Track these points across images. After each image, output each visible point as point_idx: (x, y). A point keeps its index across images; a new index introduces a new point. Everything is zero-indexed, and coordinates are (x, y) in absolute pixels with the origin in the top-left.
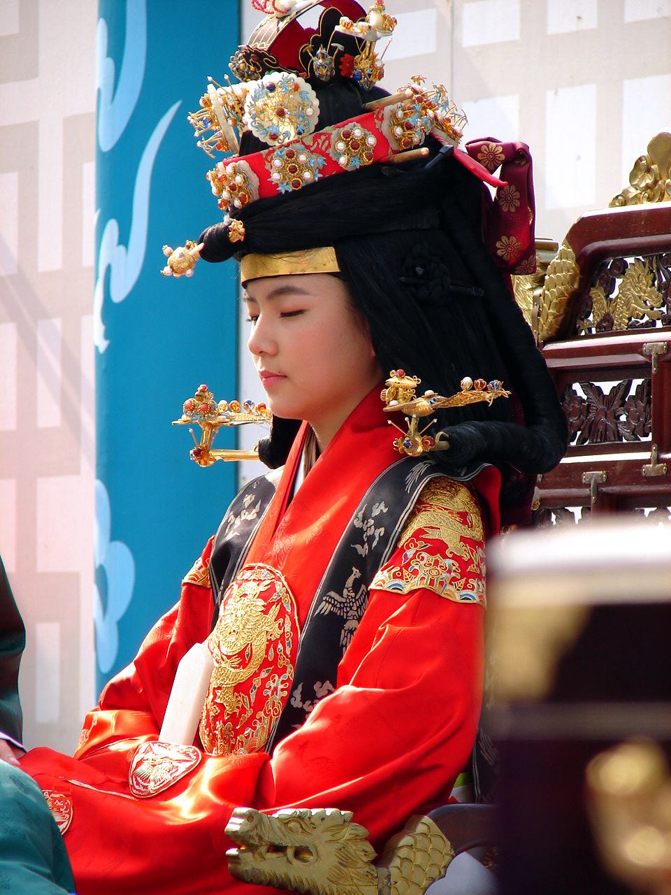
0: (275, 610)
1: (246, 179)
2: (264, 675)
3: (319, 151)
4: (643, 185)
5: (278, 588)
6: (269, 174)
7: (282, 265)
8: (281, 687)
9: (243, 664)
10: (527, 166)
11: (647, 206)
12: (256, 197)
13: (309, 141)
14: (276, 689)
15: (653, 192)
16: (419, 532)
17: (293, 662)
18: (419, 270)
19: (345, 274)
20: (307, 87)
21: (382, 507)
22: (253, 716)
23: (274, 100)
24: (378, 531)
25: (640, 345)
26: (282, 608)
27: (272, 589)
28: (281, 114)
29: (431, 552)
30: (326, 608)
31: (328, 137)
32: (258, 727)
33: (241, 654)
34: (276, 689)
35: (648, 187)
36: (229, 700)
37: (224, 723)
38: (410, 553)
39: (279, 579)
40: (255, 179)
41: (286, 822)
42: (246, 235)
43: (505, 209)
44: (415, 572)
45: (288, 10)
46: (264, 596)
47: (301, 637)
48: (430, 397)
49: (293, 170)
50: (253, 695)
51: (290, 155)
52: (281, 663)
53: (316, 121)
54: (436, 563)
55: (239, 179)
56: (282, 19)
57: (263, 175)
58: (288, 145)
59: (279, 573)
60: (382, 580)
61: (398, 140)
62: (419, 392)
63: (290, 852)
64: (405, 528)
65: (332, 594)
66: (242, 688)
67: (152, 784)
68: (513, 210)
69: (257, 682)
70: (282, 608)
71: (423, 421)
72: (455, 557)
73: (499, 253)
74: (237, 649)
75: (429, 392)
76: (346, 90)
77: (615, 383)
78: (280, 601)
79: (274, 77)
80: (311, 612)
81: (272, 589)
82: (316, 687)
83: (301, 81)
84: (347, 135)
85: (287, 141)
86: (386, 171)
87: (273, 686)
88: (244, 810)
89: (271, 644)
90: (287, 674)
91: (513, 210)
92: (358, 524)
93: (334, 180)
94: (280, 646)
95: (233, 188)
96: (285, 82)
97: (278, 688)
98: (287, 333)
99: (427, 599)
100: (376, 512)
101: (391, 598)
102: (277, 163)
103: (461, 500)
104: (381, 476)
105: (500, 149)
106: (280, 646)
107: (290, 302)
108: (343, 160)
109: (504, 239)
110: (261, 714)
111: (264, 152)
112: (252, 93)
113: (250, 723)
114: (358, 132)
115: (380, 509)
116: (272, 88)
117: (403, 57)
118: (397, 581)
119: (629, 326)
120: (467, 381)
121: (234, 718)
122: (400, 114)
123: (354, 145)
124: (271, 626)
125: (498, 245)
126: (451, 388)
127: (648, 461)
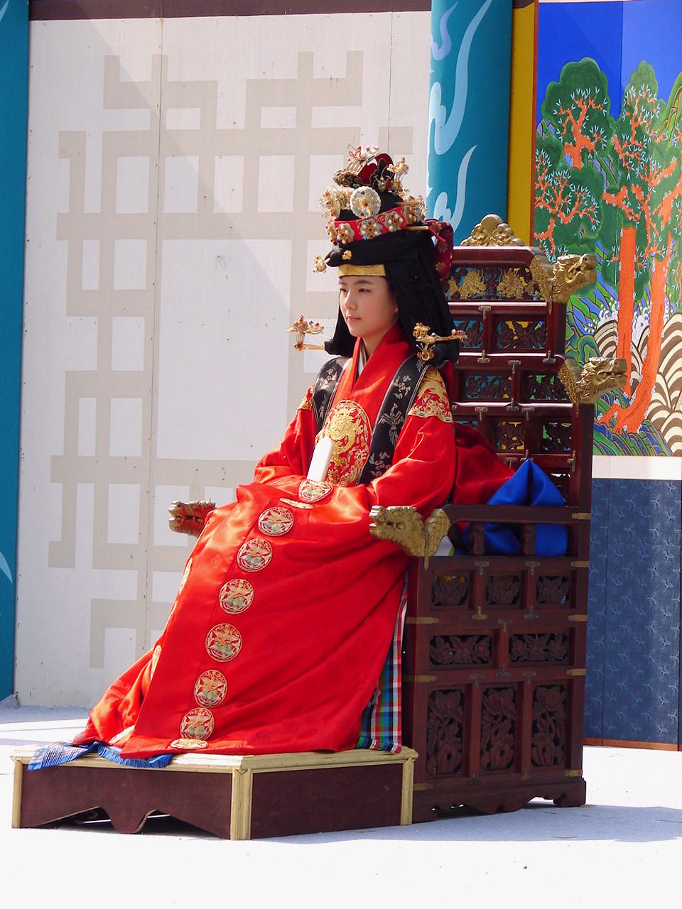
0: (358, 422)
1: (349, 232)
2: (354, 449)
3: (379, 223)
4: (479, 238)
5: (359, 412)
6: (359, 231)
7: (361, 271)
8: (363, 455)
9: (344, 444)
10: (450, 234)
12: (352, 240)
13: (376, 217)
14: (360, 456)
16: (428, 391)
17: (368, 444)
18: (416, 277)
19: (388, 277)
21: (408, 377)
23: (362, 199)
24: (407, 388)
25: (478, 306)
26: (362, 421)
27: (356, 412)
30: (383, 420)
31: (384, 216)
32: (352, 472)
34: (360, 456)
36: (337, 462)
37: (334, 470)
39: (359, 408)
41: (392, 511)
42: (351, 258)
44: (429, 409)
45: (364, 158)
47: (372, 434)
48: (434, 336)
49: (370, 230)
50: (349, 458)
52: (362, 445)
53: (379, 209)
54: (437, 405)
55: (346, 232)
56: (362, 161)
57: (357, 232)
58: (368, 219)
59: (359, 405)
61: (409, 220)
62: (429, 333)
63: (395, 525)
64: (420, 388)
65: (386, 415)
66: (343, 455)
67: (313, 497)
68: (444, 251)
69: (351, 453)
70: (362, 421)
71: (430, 345)
72: (443, 402)
73: (437, 269)
74: (340, 438)
75: (433, 334)
76: (391, 200)
77: (461, 322)
78: (361, 417)
80: (376, 423)
82: (380, 455)
83: (374, 191)
84: (393, 216)
85: (367, 217)
86: (406, 233)
87: (359, 454)
88: (378, 507)
90: (366, 449)
91: (444, 251)
92: (396, 385)
93: (386, 234)
94: (362, 437)
95: (343, 235)
96: (368, 190)
97: (361, 456)
98: (363, 300)
99: (435, 419)
100: (405, 380)
101: (418, 421)
102: (364, 226)
103: (438, 377)
104: (401, 366)
106: (362, 437)
107: (365, 287)
108: (391, 228)
109: (439, 263)
110: (353, 466)
111: (357, 221)
112: (353, 194)
113: (347, 470)
114: (397, 216)
115: (406, 378)
116: (363, 193)
118: (422, 412)
119: (468, 298)
120: (454, 331)
121: (339, 468)
122: (411, 209)
123: (396, 221)
124: (357, 428)
125: (437, 265)
126: (445, 332)
127: (481, 357)
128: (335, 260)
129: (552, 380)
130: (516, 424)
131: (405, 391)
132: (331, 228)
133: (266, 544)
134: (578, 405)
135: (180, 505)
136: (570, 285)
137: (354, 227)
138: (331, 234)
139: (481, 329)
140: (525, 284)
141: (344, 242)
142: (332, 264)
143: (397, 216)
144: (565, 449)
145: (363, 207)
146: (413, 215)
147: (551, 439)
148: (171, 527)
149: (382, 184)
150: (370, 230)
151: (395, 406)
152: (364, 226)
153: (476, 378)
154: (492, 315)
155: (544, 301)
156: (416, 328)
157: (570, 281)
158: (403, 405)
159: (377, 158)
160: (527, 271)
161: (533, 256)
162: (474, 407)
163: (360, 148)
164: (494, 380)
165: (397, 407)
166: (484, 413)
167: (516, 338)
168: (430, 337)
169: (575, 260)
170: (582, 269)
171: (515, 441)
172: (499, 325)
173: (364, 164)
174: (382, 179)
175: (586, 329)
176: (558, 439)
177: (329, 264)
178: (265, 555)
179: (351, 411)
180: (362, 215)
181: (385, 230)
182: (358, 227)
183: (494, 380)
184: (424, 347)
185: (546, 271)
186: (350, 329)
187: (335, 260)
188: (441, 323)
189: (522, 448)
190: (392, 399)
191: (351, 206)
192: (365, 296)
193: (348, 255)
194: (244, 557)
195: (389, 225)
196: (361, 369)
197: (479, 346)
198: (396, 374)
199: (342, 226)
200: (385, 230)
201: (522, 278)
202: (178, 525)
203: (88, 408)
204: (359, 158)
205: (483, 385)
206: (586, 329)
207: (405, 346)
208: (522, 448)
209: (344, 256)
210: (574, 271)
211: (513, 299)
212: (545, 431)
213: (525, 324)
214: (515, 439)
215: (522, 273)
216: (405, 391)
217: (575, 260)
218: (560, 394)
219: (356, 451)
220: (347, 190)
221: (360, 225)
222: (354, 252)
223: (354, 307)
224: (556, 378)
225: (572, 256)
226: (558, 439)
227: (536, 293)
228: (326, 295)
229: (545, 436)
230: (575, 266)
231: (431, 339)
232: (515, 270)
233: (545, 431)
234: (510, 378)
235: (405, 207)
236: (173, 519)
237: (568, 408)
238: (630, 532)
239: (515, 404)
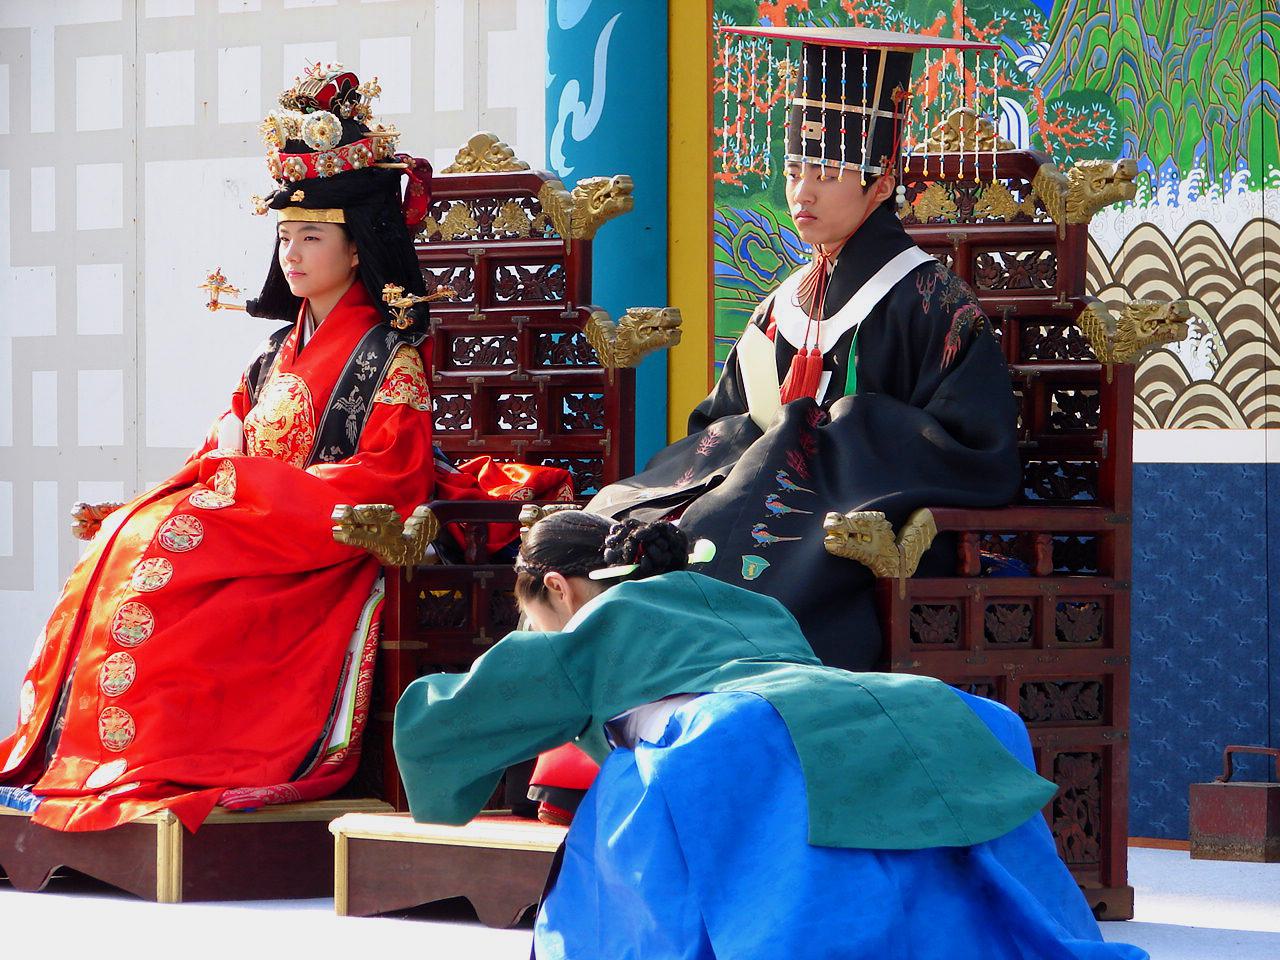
0: (298, 398)
1: (301, 167)
4: (465, 162)
7: (312, 215)
9: (281, 427)
11: (472, 174)
15: (470, 166)
16: (397, 371)
19: (346, 228)
20: (337, 119)
21: (373, 354)
22: (292, 455)
27: (296, 386)
28: (323, 133)
29: (406, 381)
33: (279, 422)
35: (469, 163)
38: (394, 382)
40: (306, 168)
42: (304, 200)
43: (414, 195)
44: (398, 393)
46: (292, 390)
49: (329, 166)
51: (330, 158)
52: (304, 426)
55: (297, 167)
57: (311, 167)
60: (379, 396)
61: (379, 154)
62: (404, 295)
69: (290, 436)
71: (408, 308)
74: (277, 420)
75: (410, 295)
76: (354, 130)
79: (320, 113)
81: (296, 386)
83: (333, 116)
84: (360, 151)
89: (297, 416)
90: (308, 432)
93: (349, 172)
94: (302, 417)
98: (310, 251)
99: (407, 409)
100: (370, 358)
101: (386, 409)
105: (414, 162)
106: (302, 417)
108: (356, 165)
114: (364, 150)
115: (372, 356)
116: (319, 119)
117: (381, 113)
118: (388, 398)
123: (363, 156)
127: (473, 313)
128: (280, 202)
129: (574, 339)
130: (524, 397)
131: (369, 372)
132: (274, 161)
133: (197, 524)
134: (611, 371)
135: (84, 507)
136: (596, 217)
137: (307, 162)
138: (274, 168)
139: (472, 277)
140: (531, 217)
141: (292, 179)
142: (273, 206)
143: (364, 150)
144: (596, 427)
145: (318, 135)
146: (384, 148)
147: (575, 414)
148: (74, 533)
149: (345, 109)
150: (329, 166)
151: (356, 389)
152: (322, 161)
153: (467, 340)
154: (486, 259)
155: (560, 239)
156: (384, 291)
157: (595, 212)
158: (368, 389)
159: (339, 79)
160: (535, 200)
161: (542, 182)
162: (465, 378)
163: (319, 64)
164: (493, 341)
165: (358, 390)
166: (479, 384)
167: (521, 287)
168: (406, 299)
169: (605, 184)
170: (612, 194)
171: (524, 419)
172: (498, 271)
173: (324, 83)
174: (347, 103)
175: (801, 256)
176: (585, 415)
177: (272, 206)
178: (194, 535)
179: (291, 386)
180: (318, 146)
181: (347, 166)
182: (313, 162)
183: (493, 341)
184: (398, 313)
185: (560, 200)
186: (292, 288)
187: (280, 202)
188: (413, 282)
189: (534, 426)
190: (350, 381)
191: (302, 136)
192: (311, 245)
193: (298, 196)
194: (168, 534)
195: (354, 160)
196: (307, 339)
197: (470, 299)
198: (359, 346)
199: (291, 160)
200: (347, 166)
201: (527, 211)
202: (85, 530)
203: (45, 384)
204: (317, 76)
205: (477, 348)
206: (801, 256)
207: (371, 311)
208: (534, 426)
209: (294, 196)
210: (602, 199)
211: (515, 238)
212: (566, 404)
213: (533, 269)
214: (523, 415)
215: (527, 204)
216: (369, 372)
217: (605, 184)
218: (585, 352)
219: (296, 434)
220: (297, 115)
221: (316, 160)
222: (307, 190)
223: (812, 199)
224: (579, 337)
225: (598, 179)
226: (585, 415)
227: (548, 228)
228: (248, 238)
229: (567, 410)
230: (602, 191)
231: (408, 301)
232: (517, 200)
233: (566, 404)
234: (514, 339)
235: (375, 139)
236: (77, 523)
237: (597, 375)
238: (1162, 828)
239: (523, 372)
